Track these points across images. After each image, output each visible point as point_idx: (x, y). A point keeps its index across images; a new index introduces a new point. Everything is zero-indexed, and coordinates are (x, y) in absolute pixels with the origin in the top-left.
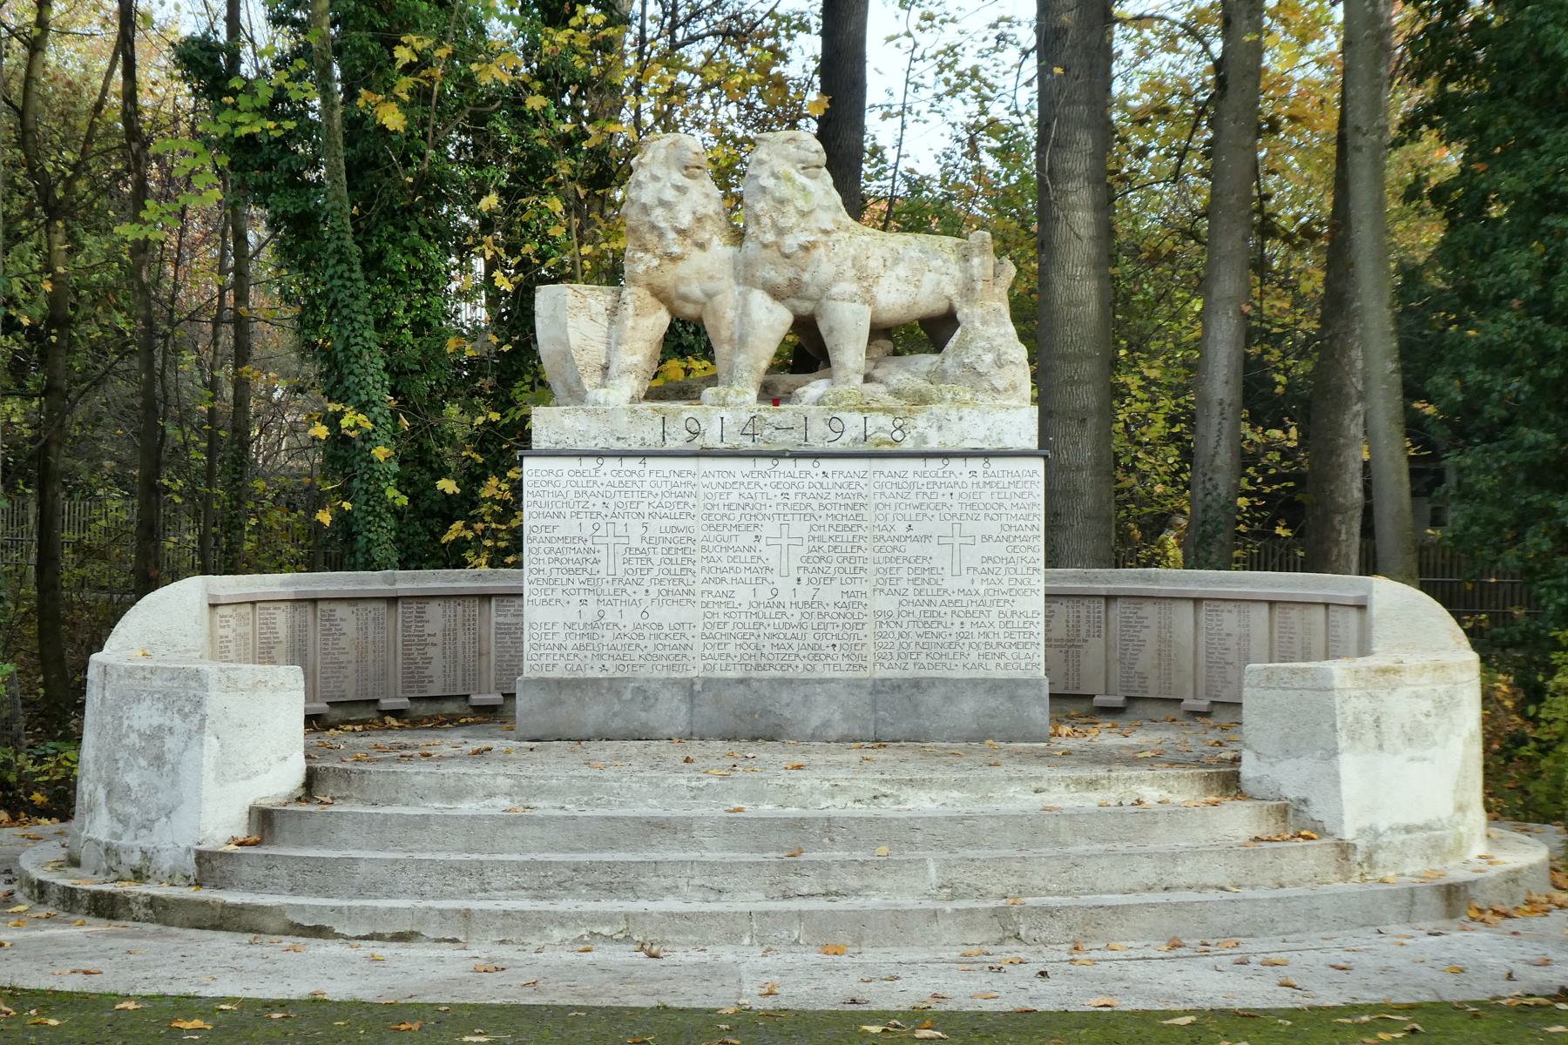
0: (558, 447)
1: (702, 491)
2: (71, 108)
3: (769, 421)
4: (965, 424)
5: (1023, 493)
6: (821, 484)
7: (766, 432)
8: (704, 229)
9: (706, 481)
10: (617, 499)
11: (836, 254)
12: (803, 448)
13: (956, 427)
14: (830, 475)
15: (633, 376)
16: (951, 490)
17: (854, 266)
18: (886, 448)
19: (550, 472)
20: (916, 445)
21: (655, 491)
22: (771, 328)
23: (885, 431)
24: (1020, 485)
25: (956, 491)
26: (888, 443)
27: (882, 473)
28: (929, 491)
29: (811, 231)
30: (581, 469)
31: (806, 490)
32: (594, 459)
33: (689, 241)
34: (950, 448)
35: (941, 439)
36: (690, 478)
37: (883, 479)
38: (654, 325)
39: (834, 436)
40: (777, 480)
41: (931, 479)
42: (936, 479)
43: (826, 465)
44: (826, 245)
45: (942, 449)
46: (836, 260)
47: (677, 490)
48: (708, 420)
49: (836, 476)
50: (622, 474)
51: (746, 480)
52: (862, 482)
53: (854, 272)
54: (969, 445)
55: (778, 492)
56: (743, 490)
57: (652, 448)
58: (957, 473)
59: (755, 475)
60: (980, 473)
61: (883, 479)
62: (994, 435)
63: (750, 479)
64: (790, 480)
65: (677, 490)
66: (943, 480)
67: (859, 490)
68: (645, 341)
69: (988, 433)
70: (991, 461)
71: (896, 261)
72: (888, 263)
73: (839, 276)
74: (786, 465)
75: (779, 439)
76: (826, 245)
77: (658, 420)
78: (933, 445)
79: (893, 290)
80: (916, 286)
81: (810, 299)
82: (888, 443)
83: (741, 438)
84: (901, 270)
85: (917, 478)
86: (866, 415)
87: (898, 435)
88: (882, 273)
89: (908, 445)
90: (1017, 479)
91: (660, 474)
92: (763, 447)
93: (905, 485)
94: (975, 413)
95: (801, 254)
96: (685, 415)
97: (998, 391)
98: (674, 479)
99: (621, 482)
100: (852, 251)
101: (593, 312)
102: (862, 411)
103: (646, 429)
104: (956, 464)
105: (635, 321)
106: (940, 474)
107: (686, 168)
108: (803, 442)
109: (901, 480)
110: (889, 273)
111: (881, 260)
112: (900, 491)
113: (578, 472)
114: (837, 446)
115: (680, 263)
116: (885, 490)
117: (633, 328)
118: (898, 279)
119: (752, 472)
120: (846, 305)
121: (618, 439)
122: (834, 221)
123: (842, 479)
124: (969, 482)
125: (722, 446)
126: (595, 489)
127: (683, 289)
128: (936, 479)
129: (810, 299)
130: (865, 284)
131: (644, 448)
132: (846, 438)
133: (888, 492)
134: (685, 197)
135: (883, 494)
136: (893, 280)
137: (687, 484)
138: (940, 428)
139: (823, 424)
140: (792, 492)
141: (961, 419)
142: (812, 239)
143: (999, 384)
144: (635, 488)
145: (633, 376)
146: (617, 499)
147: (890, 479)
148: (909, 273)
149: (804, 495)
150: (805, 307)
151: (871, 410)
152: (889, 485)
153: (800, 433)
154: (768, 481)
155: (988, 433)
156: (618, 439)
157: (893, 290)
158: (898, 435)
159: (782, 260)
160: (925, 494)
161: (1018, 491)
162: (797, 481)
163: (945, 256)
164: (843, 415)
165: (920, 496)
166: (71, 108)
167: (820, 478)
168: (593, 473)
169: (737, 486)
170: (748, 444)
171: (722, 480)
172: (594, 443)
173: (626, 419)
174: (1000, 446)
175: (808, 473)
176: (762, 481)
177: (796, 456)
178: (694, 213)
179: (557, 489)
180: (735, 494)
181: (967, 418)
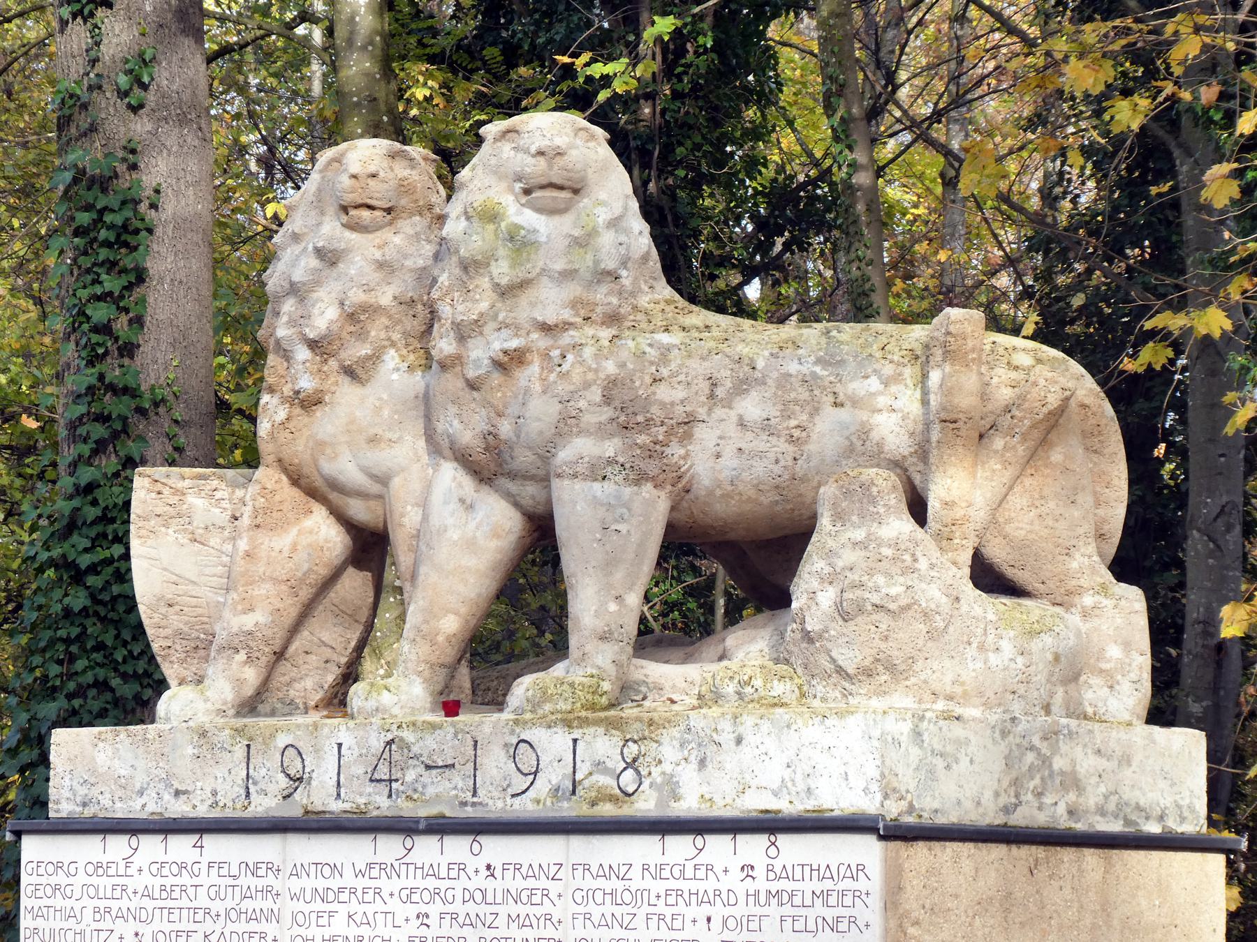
0: (88, 812)
1: (289, 907)
2: (1202, 19)
3: (416, 749)
4: (746, 752)
5: (838, 919)
6: (484, 893)
7: (410, 776)
8: (361, 335)
9: (295, 884)
10: (156, 926)
11: (564, 376)
12: (469, 812)
13: (732, 760)
14: (498, 873)
15: (242, 656)
16: (706, 910)
17: (607, 399)
18: (607, 810)
19: (58, 866)
20: (660, 803)
21: (217, 907)
22: (470, 545)
23: (606, 771)
24: (833, 900)
25: (718, 912)
26: (612, 799)
27: (586, 867)
28: (668, 912)
29: (518, 328)
30: (105, 859)
31: (457, 907)
32: (125, 838)
33: (333, 363)
34: (720, 810)
35: (705, 789)
36: (271, 879)
37: (590, 883)
38: (294, 548)
39: (520, 783)
40: (411, 883)
41: (672, 884)
42: (680, 884)
43: (497, 849)
44: (546, 356)
45: (706, 812)
46: (562, 388)
47: (248, 905)
48: (317, 750)
49: (509, 874)
50: (165, 871)
51: (361, 883)
52: (554, 888)
53: (607, 413)
54: (753, 803)
55: (412, 910)
56: (354, 906)
57: (228, 813)
58: (718, 869)
59: (375, 873)
60: (760, 872)
61: (590, 883)
62: (799, 777)
63: (366, 882)
64: (431, 883)
65: (248, 905)
66: (694, 886)
67: (547, 907)
68: (275, 581)
69: (787, 774)
70: (783, 840)
71: (742, 387)
72: (720, 392)
73: (567, 425)
74: (427, 849)
75: (431, 791)
76: (546, 356)
77: (240, 752)
78: (688, 806)
79: (729, 451)
80: (791, 440)
81: (527, 477)
82: (612, 799)
83: (370, 788)
84: (752, 407)
85: (649, 883)
86: (577, 734)
87: (628, 778)
88: (702, 412)
89: (646, 805)
90: (828, 884)
91: (224, 872)
92: (406, 809)
93: (627, 897)
94: (766, 726)
95: (497, 378)
96: (282, 740)
97: (848, 677)
98: (247, 880)
99: (163, 888)
100: (610, 367)
101: (198, 522)
102: (568, 724)
103: (220, 772)
104: (718, 844)
105: (251, 539)
106: (689, 873)
107: (345, 209)
108: (468, 796)
109: (620, 885)
110: (719, 412)
111: (705, 386)
112: (618, 911)
113: (98, 866)
114: (525, 808)
115: (319, 412)
116: (592, 907)
117: (248, 555)
118: (742, 424)
119: (370, 866)
120: (579, 485)
121: (178, 793)
122: (575, 304)
123: (520, 883)
124: (740, 888)
125: (336, 806)
126: (124, 903)
127: (328, 468)
128: (680, 884)
129: (527, 477)
130: (642, 439)
131: (216, 814)
132: (542, 787)
133: (596, 912)
134: (334, 272)
135: (587, 917)
136: (731, 429)
137: (267, 890)
138: (702, 763)
139: (502, 753)
140: (435, 909)
141: (739, 741)
142: (514, 344)
143: (849, 658)
144: (185, 902)
145: (242, 656)
146: (156, 926)
147: (601, 883)
148: (774, 412)
149: (454, 917)
150: (530, 492)
151: (584, 722)
152: (599, 895)
153: (465, 777)
154: (395, 884)
155: (787, 774)
156: (178, 793)
157: (729, 451)
158: (628, 778)
159: (467, 395)
160: (661, 918)
161: (830, 914)
162: (443, 885)
163: (888, 370)
164: (536, 735)
165: (653, 922)
166: (1202, 19)
167: (480, 881)
168: (122, 864)
169: (344, 897)
170: (381, 804)
171: (321, 884)
172: (140, 802)
173: (190, 751)
174: (810, 804)
175: (462, 868)
176: (387, 885)
177: (441, 827)
178: (342, 304)
179: (68, 903)
180: (340, 919)
181: (749, 738)
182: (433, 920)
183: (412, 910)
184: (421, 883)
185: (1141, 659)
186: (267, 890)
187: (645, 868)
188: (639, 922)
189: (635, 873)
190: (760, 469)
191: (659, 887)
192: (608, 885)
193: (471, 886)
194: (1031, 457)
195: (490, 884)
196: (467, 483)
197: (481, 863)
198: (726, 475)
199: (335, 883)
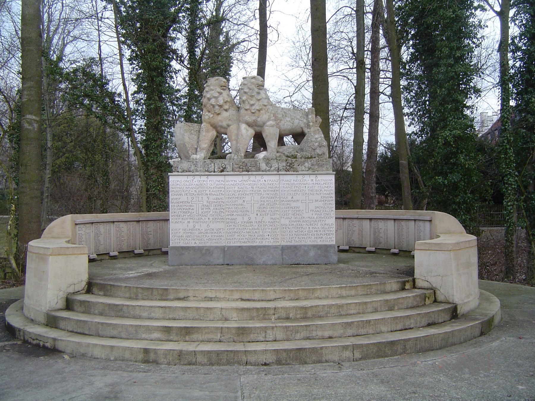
16: (305, 186)
21: (211, 186)
27: (283, 180)
55: (250, 186)
73: (269, 119)
85: (294, 182)
106: (302, 180)
109: (289, 183)
126: (192, 186)
150: (258, 129)
154: (247, 183)
162: (256, 183)
171: (232, 183)
178: (224, 100)
182: (255, 188)
183: (250, 186)
184: (252, 183)
185: (329, 9)
186: (221, 184)
187: (294, 180)
188: (293, 187)
189: (292, 181)
190: (289, 127)
191: (296, 183)
192: (287, 183)
193: (261, 183)
194: (64, 352)
195: (265, 183)
196: (247, 127)
197: (263, 180)
198: (285, 128)
199: (235, 183)
